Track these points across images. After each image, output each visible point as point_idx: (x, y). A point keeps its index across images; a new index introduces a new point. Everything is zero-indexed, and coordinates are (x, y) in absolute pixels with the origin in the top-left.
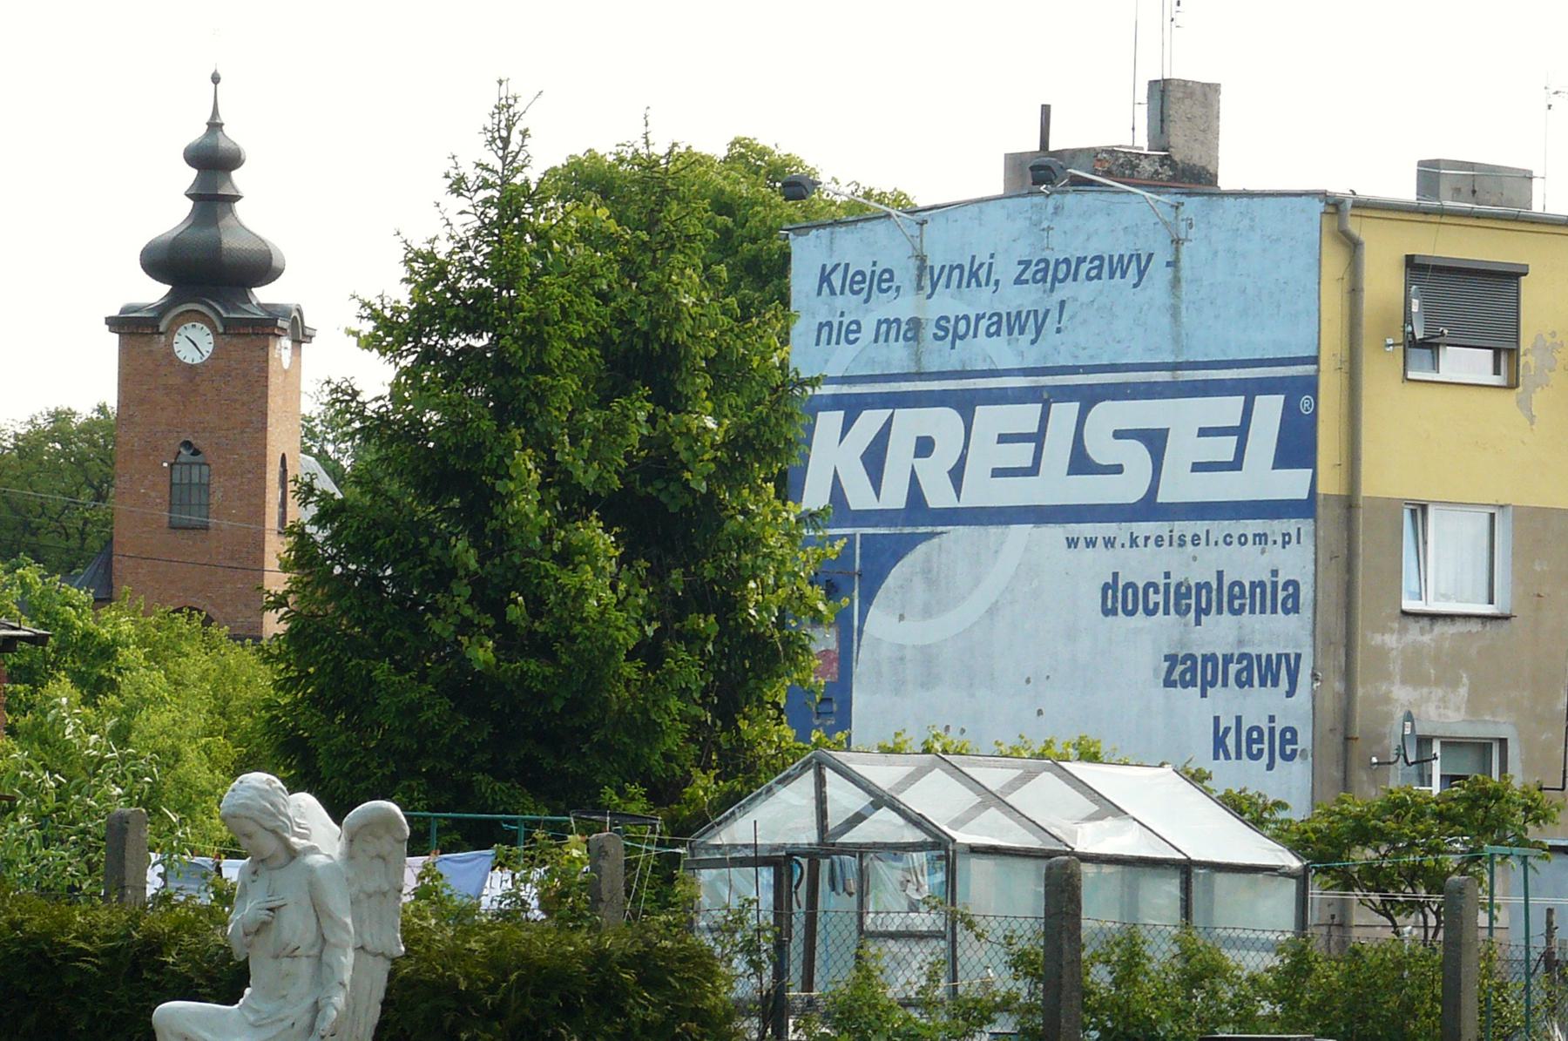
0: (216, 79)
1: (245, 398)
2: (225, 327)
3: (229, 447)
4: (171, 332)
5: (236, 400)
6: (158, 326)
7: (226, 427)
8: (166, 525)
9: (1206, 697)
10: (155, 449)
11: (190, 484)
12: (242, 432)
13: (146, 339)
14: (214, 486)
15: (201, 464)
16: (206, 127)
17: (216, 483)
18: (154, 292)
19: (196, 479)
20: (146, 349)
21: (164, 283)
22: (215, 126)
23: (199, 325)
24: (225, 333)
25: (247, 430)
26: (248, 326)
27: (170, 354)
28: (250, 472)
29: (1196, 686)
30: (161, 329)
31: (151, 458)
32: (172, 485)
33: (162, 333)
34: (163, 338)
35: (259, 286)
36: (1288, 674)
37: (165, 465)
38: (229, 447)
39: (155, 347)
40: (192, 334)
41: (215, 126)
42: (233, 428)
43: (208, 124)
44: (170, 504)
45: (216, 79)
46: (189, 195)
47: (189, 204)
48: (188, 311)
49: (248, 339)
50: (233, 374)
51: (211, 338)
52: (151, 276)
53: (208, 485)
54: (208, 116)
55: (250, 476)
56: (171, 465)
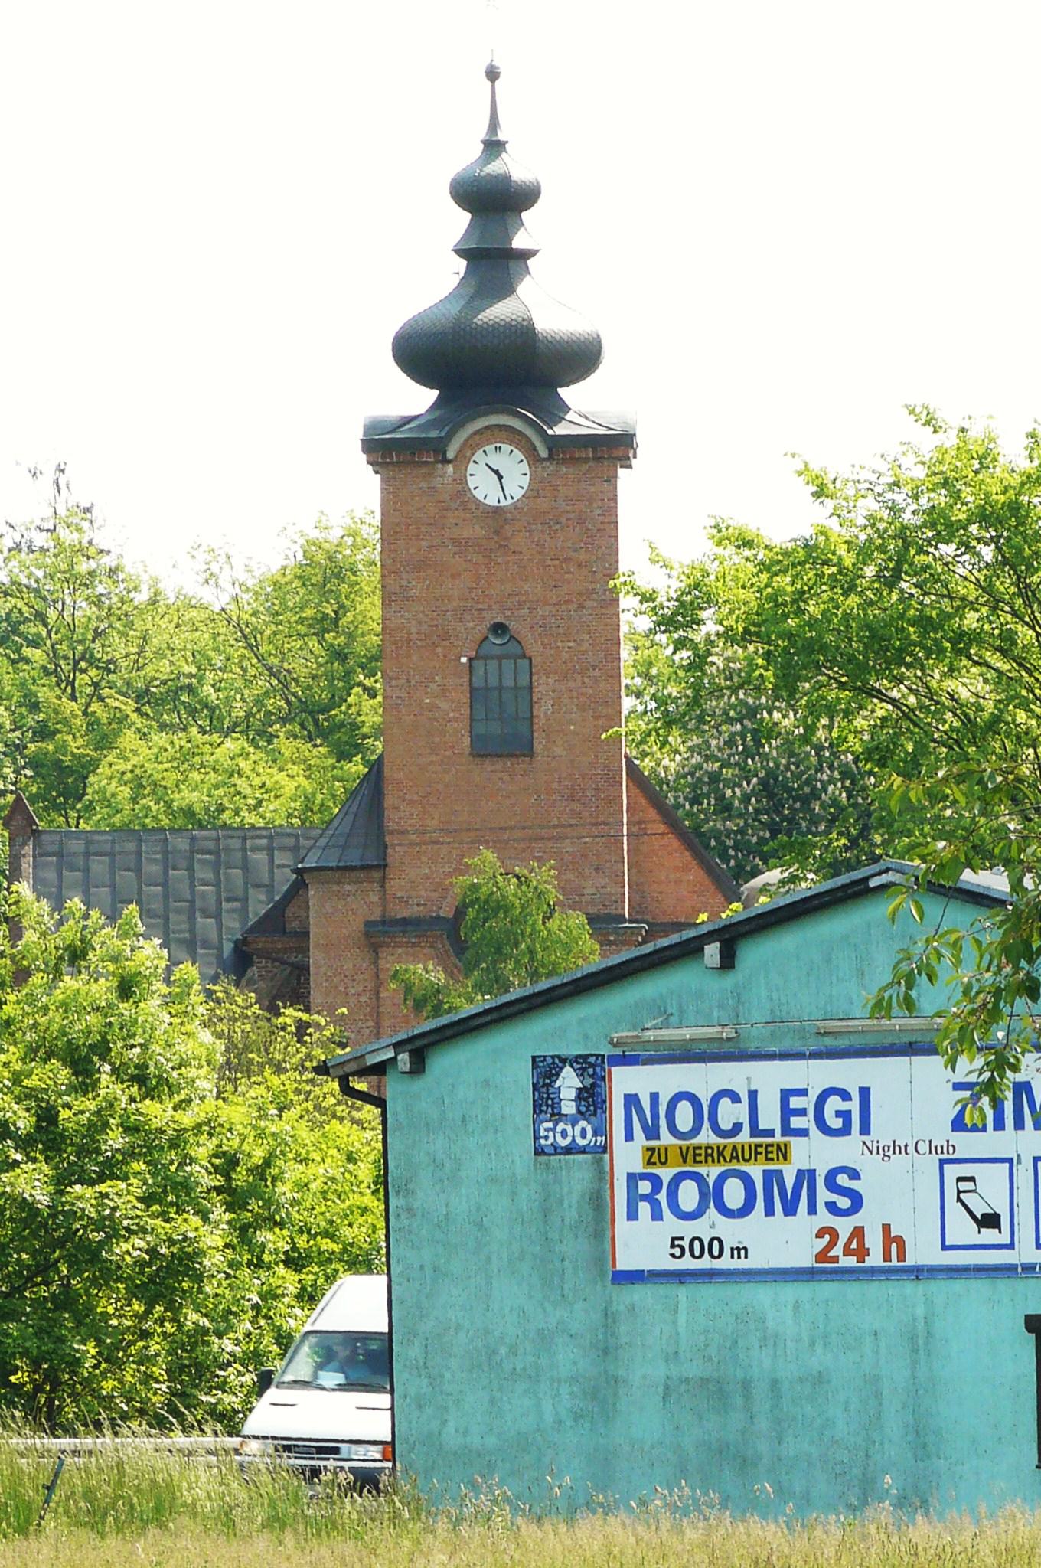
0: (492, 75)
1: (582, 556)
2: (550, 450)
3: (561, 630)
4: (463, 459)
5: (567, 560)
6: (445, 453)
7: (554, 600)
8: (467, 751)
9: (636, 1218)
10: (446, 636)
11: (500, 688)
12: (581, 607)
13: (424, 470)
14: (539, 690)
15: (516, 657)
16: (482, 146)
17: (544, 685)
18: (419, 399)
19: (509, 682)
20: (424, 485)
21: (432, 388)
22: (493, 147)
23: (506, 448)
24: (550, 458)
25: (588, 603)
26: (586, 447)
27: (462, 493)
28: (594, 667)
29: (751, 1136)
30: (450, 455)
31: (439, 650)
32: (472, 690)
33: (449, 462)
34: (450, 469)
35: (573, 382)
36: (644, 1132)
37: (464, 660)
38: (561, 630)
39: (438, 482)
40: (495, 460)
41: (493, 147)
42: (567, 602)
43: (482, 142)
44: (472, 720)
45: (492, 75)
46: (460, 252)
47: (462, 264)
48: (487, 428)
49: (585, 467)
50: (563, 520)
51: (525, 467)
52: (412, 378)
53: (531, 687)
54: (482, 131)
55: (597, 673)
56: (470, 660)
